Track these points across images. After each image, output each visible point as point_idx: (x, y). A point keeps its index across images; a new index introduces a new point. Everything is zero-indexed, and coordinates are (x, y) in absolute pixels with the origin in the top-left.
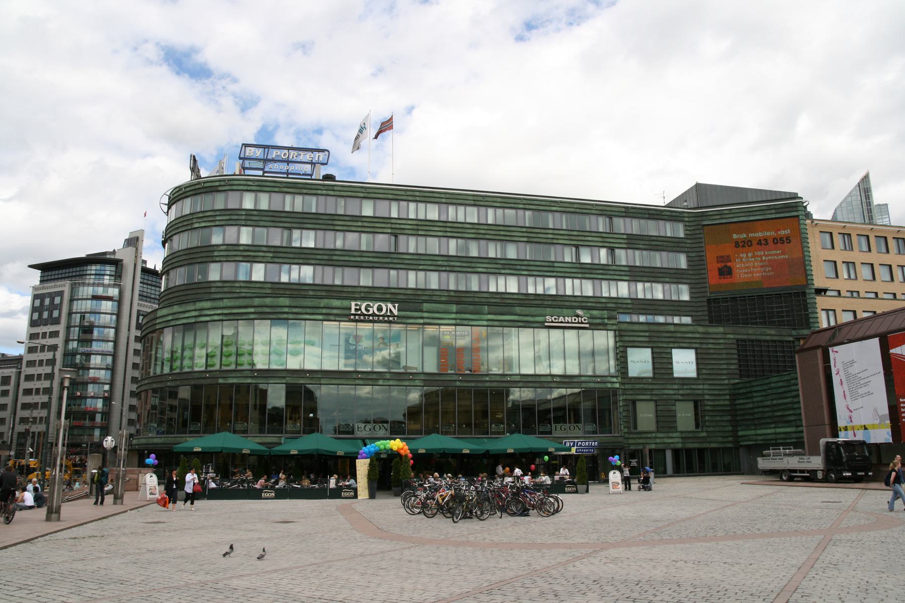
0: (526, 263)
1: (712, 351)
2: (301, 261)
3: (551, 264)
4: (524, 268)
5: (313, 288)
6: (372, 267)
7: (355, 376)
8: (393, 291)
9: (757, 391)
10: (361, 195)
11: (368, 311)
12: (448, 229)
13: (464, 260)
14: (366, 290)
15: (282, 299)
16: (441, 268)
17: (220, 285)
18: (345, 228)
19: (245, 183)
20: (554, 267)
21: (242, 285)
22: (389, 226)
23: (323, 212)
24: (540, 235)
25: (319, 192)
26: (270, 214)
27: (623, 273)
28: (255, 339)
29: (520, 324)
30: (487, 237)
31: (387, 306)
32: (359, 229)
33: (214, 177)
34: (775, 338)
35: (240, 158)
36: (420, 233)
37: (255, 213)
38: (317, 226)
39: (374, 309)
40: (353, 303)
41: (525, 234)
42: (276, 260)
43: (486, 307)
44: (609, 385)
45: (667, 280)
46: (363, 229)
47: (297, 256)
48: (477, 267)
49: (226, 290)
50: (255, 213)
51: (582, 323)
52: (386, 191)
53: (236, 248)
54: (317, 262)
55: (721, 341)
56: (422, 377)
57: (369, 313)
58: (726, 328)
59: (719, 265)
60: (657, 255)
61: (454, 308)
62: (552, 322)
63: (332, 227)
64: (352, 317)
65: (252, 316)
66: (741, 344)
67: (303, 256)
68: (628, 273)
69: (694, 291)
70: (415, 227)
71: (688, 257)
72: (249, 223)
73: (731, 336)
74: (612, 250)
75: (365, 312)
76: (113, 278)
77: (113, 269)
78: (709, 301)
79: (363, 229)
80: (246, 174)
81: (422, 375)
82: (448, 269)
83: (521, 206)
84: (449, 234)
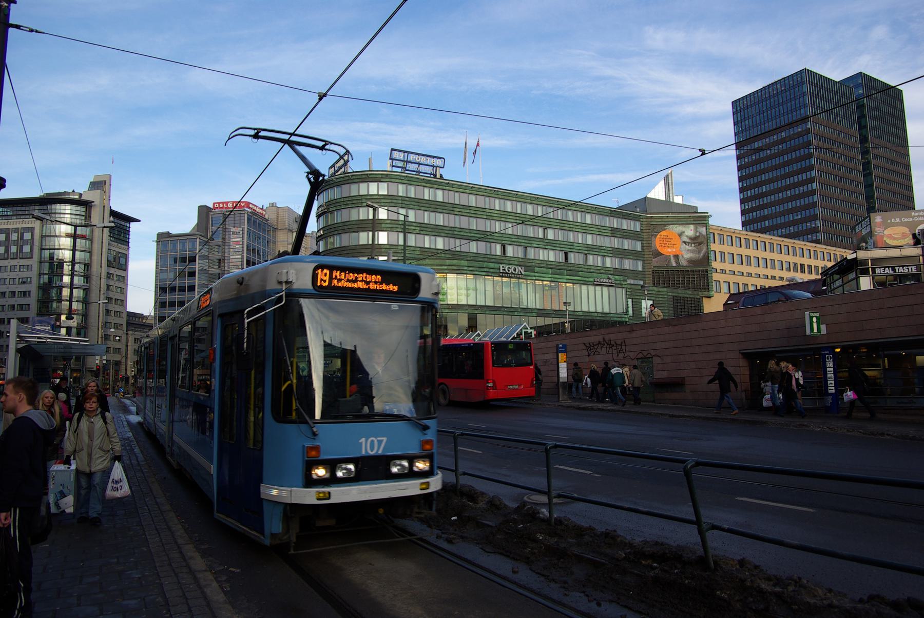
0: (559, 242)
1: (661, 302)
2: (436, 234)
3: (572, 244)
4: (558, 245)
7: (503, 309)
8: (488, 256)
11: (509, 271)
12: (518, 218)
13: (526, 238)
14: (474, 255)
16: (514, 244)
18: (460, 213)
19: (399, 177)
20: (573, 246)
22: (485, 214)
25: (444, 188)
27: (609, 252)
29: (582, 282)
30: (538, 224)
32: (469, 215)
34: (691, 296)
35: (390, 159)
36: (502, 219)
37: (407, 199)
38: (444, 211)
39: (512, 270)
41: (558, 224)
42: (422, 232)
43: (565, 271)
44: (624, 319)
45: (631, 257)
46: (471, 215)
51: (612, 283)
52: (483, 190)
53: (397, 222)
54: (446, 235)
55: (666, 296)
56: (536, 311)
58: (668, 289)
60: (626, 241)
62: (598, 282)
65: (446, 271)
66: (675, 299)
68: (611, 252)
70: (499, 215)
72: (404, 206)
73: (670, 294)
75: (508, 272)
76: (84, 218)
77: (83, 209)
78: (653, 272)
79: (471, 215)
80: (394, 170)
82: (518, 244)
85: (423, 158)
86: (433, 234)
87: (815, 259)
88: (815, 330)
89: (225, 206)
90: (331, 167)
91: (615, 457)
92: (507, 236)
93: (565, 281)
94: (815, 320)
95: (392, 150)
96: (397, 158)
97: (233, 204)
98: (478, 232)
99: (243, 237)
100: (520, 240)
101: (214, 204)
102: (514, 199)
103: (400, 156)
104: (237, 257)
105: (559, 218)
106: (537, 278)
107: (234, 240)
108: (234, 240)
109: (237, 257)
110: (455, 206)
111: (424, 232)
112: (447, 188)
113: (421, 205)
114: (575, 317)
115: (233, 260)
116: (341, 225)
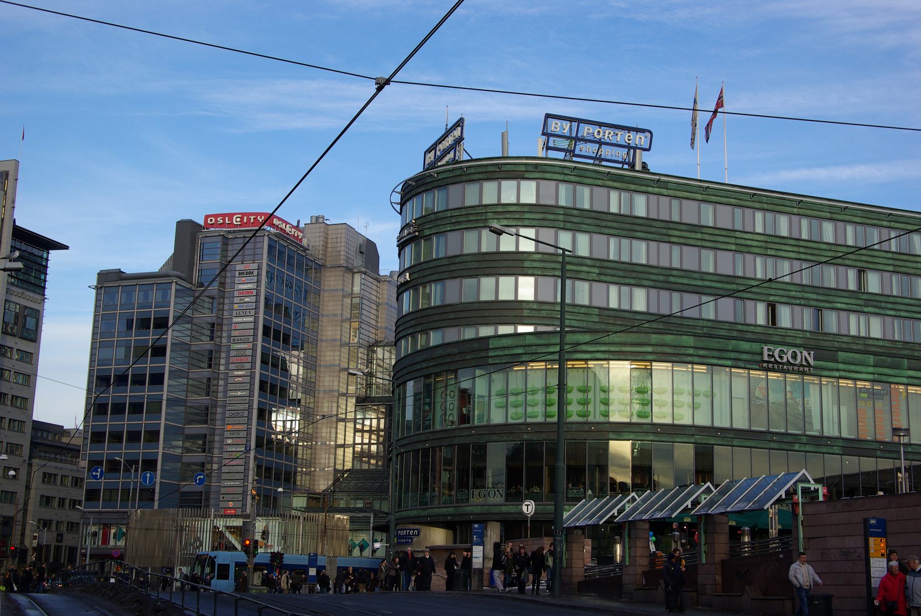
0: (892, 299)
2: (632, 281)
4: (890, 306)
6: (718, 295)
8: (740, 327)
9: (197, 512)
10: (699, 197)
11: (781, 357)
12: (802, 250)
13: (821, 291)
14: (709, 324)
15: (685, 337)
16: (794, 301)
17: (535, 307)
18: (682, 241)
22: (733, 240)
23: (655, 217)
24: (908, 264)
25: (650, 189)
26: (593, 215)
31: (801, 352)
32: (699, 243)
33: (527, 158)
35: (543, 134)
37: (575, 212)
38: (650, 236)
40: (766, 348)
41: (891, 262)
42: (603, 278)
43: (906, 360)
46: (704, 244)
47: (627, 274)
48: (835, 302)
49: (544, 313)
50: (575, 212)
56: (840, 443)
57: (783, 361)
61: (871, 359)
63: (666, 239)
64: (765, 365)
67: (634, 275)
70: (763, 244)
72: (569, 225)
74: (861, 272)
79: (704, 244)
80: (549, 156)
81: (840, 440)
82: (802, 302)
83: (885, 223)
84: (803, 256)
86: (626, 281)
90: (429, 151)
93: (905, 380)
97: (242, 218)
98: (717, 278)
99: (258, 281)
104: (245, 319)
106: (843, 374)
107: (241, 287)
109: (245, 319)
111: (608, 279)
112: (656, 190)
113: (603, 224)
115: (239, 326)
116: (445, 262)
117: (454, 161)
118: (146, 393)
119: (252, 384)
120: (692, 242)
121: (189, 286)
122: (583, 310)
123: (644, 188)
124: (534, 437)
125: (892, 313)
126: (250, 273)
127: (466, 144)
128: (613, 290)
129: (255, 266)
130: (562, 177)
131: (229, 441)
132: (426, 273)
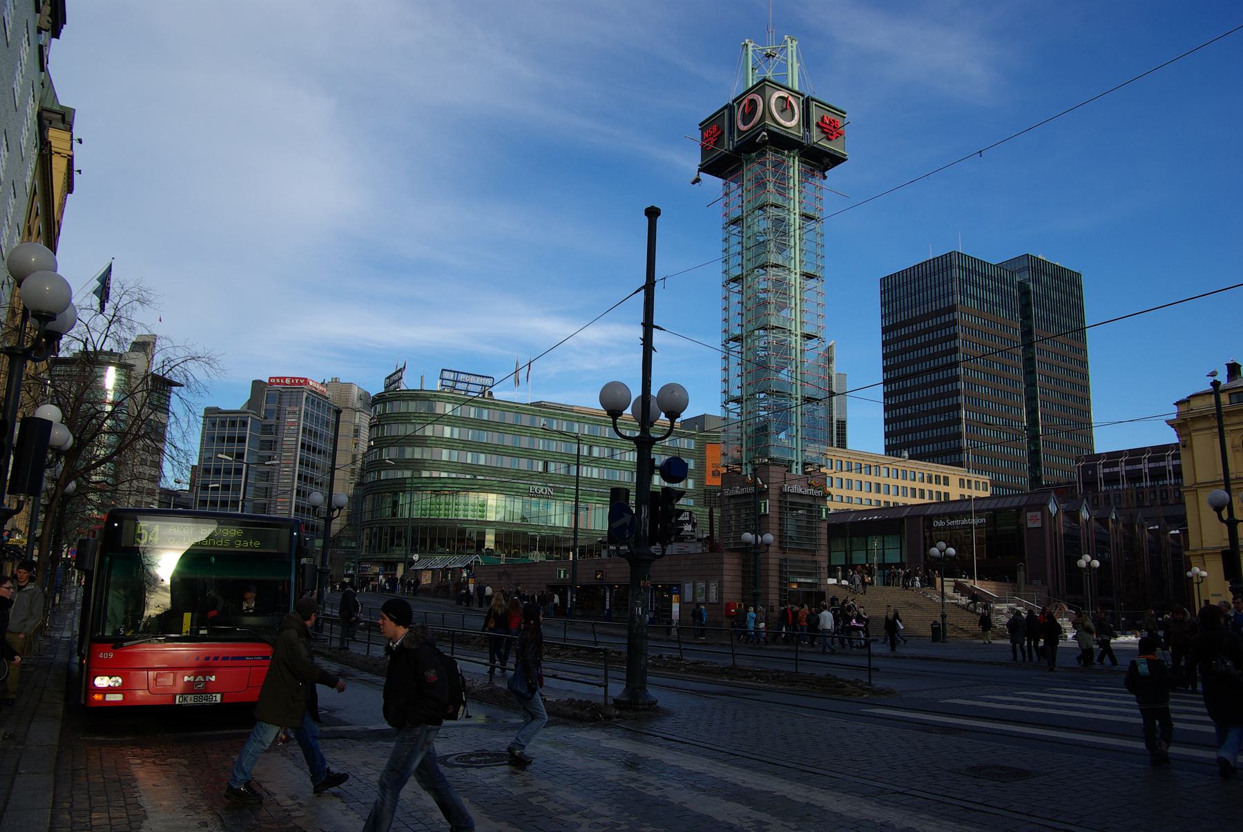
2: (479, 451)
5: (485, 468)
14: (515, 471)
21: (445, 463)
22: (529, 432)
25: (490, 407)
28: (945, 591)
32: (512, 433)
36: (546, 437)
37: (453, 417)
38: (489, 429)
42: (465, 449)
46: (515, 433)
50: (453, 417)
53: (442, 439)
59: (714, 469)
69: (697, 483)
71: (695, 462)
79: (515, 433)
85: (473, 377)
86: (476, 450)
87: (903, 479)
88: (562, 576)
89: (282, 381)
90: (387, 378)
91: (784, 706)
92: (550, 453)
93: (595, 502)
94: (562, 572)
95: (443, 370)
96: (447, 378)
97: (291, 381)
98: (520, 449)
99: (300, 418)
100: (564, 458)
101: (270, 378)
102: (561, 417)
103: (451, 375)
105: (607, 436)
106: (566, 498)
107: (289, 420)
108: (289, 420)
110: (500, 424)
111: (468, 449)
112: (493, 407)
114: (587, 535)
115: (287, 443)
116: (390, 438)
117: (395, 390)
118: (232, 479)
119: (294, 476)
120: (509, 432)
121: (258, 418)
122: (455, 464)
123: (487, 406)
124: (424, 525)
125: (604, 466)
126: (294, 413)
127: (404, 380)
128: (469, 455)
129: (298, 409)
130: (448, 401)
131: (279, 508)
132: (381, 442)
